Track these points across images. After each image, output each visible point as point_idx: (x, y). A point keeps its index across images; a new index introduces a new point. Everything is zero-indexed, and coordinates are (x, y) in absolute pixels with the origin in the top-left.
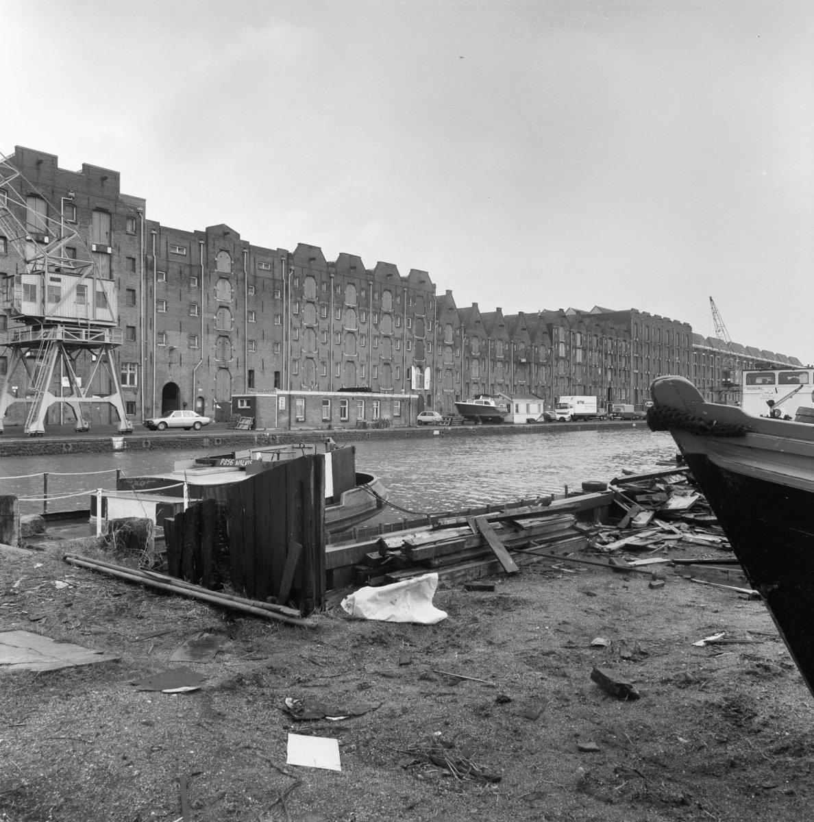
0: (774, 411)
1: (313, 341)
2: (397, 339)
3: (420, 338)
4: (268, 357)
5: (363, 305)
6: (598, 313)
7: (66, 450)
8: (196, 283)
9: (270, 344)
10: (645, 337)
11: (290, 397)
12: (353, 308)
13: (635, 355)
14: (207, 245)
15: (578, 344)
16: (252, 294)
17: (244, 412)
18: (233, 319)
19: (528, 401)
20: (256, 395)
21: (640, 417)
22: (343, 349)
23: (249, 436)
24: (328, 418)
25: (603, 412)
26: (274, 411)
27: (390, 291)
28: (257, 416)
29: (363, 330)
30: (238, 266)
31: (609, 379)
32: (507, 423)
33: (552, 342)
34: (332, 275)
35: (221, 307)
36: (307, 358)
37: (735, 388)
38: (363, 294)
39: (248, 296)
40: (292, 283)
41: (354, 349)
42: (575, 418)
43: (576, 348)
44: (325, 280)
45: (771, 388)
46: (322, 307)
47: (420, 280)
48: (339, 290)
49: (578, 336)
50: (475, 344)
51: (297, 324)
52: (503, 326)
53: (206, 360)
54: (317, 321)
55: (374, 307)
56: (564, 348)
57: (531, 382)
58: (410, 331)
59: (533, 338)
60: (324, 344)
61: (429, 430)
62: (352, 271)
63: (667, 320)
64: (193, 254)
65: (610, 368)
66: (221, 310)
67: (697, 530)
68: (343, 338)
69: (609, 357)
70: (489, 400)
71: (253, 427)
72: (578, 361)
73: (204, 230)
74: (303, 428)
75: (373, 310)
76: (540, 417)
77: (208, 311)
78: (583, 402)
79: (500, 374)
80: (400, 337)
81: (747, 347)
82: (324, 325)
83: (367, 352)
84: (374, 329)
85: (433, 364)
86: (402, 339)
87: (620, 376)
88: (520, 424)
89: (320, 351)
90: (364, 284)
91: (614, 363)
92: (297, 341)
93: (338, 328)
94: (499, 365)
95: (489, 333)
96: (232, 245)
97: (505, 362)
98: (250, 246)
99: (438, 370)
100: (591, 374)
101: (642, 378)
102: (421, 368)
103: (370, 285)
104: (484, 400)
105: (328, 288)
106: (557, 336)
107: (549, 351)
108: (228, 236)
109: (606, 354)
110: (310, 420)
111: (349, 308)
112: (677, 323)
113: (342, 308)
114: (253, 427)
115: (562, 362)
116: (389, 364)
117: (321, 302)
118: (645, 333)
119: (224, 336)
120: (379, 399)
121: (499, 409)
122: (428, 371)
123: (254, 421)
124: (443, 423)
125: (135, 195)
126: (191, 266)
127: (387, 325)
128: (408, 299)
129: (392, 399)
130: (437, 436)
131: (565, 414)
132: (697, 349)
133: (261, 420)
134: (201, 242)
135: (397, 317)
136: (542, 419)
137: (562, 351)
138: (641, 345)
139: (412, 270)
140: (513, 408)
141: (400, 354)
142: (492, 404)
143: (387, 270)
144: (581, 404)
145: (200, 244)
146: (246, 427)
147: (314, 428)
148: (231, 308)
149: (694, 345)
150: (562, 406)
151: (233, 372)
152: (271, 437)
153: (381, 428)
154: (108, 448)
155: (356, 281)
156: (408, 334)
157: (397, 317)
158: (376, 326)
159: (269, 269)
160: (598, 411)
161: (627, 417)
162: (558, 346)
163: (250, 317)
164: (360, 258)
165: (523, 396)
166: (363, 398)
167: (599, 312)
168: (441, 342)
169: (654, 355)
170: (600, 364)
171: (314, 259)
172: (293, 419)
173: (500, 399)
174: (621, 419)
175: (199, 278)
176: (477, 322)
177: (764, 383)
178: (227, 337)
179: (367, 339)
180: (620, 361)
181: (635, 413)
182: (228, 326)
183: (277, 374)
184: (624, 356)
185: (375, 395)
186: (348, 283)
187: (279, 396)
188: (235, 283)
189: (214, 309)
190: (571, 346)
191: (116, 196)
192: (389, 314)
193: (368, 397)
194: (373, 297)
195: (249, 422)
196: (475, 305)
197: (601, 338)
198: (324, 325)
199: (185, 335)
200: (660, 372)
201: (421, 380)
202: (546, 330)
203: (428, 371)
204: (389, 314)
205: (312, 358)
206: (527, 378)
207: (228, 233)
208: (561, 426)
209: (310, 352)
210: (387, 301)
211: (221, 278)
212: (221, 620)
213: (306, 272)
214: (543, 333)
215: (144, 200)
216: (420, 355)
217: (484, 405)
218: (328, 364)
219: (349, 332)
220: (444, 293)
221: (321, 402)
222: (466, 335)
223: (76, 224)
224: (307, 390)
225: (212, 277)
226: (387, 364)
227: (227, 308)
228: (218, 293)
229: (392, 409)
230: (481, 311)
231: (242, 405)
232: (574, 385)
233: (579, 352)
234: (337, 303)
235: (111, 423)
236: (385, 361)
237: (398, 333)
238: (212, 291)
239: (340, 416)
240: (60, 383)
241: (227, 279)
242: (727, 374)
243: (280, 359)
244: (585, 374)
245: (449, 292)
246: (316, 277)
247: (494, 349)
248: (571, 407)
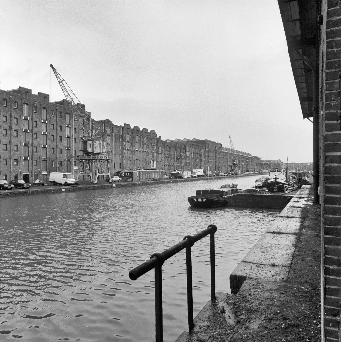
1: (128, 153)
5: (140, 142)
7: (53, 192)
11: (139, 172)
14: (104, 125)
17: (129, 177)
30: (111, 131)
36: (127, 159)
37: (236, 165)
38: (140, 138)
42: (199, 176)
43: (191, 153)
44: (131, 134)
47: (153, 132)
49: (192, 149)
50: (166, 153)
58: (151, 149)
59: (181, 150)
63: (215, 143)
67: (42, 329)
70: (179, 171)
71: (132, 181)
81: (226, 148)
93: (134, 149)
95: (170, 149)
98: (114, 125)
99: (158, 161)
105: (132, 137)
113: (135, 143)
120: (157, 172)
123: (132, 179)
127: (146, 148)
130: (63, 192)
132: (223, 152)
135: (148, 145)
139: (151, 130)
143: (145, 130)
145: (103, 125)
154: (112, 187)
155: (138, 135)
157: (148, 145)
172: (140, 179)
185: (156, 171)
187: (137, 172)
190: (190, 153)
191: (84, 112)
195: (131, 179)
203: (155, 162)
206: (179, 163)
207: (110, 122)
213: (127, 132)
215: (91, 113)
219: (137, 150)
220: (159, 137)
223: (37, 113)
225: (106, 135)
226: (145, 160)
227: (109, 144)
228: (107, 140)
233: (192, 154)
235: (84, 180)
240: (73, 168)
242: (234, 161)
244: (194, 161)
245: (160, 137)
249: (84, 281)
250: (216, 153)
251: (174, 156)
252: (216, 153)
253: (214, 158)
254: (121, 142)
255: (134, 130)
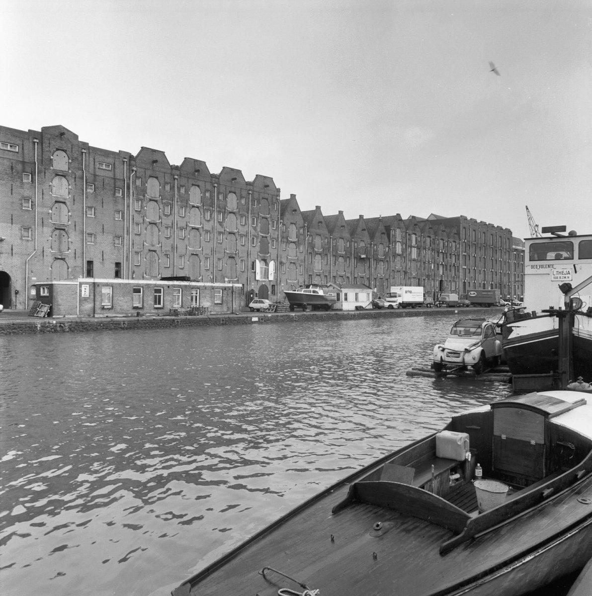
0: (571, 301)
2: (241, 236)
3: (264, 235)
4: (108, 249)
5: (207, 205)
6: (433, 219)
8: (30, 179)
9: (110, 237)
10: (472, 239)
11: (94, 285)
12: (198, 207)
13: (464, 253)
15: (414, 243)
16: (92, 191)
18: (70, 214)
19: (357, 290)
20: (53, 283)
21: (464, 304)
22: (188, 244)
23: (30, 324)
24: (140, 306)
25: (430, 300)
26: (75, 298)
27: (235, 193)
28: (55, 304)
29: (208, 226)
31: (441, 273)
32: (337, 310)
33: (389, 241)
34: (176, 177)
35: (56, 202)
36: (150, 251)
38: (208, 195)
39: (86, 193)
40: (134, 182)
41: (198, 243)
42: (404, 305)
43: (411, 247)
44: (168, 180)
45: (567, 266)
46: (166, 205)
48: (183, 191)
49: (414, 237)
50: (318, 241)
51: (138, 218)
52: (344, 226)
53: (40, 252)
54: (160, 218)
55: (219, 207)
56: (400, 247)
57: (370, 274)
58: (255, 229)
59: (372, 237)
60: (167, 238)
61: (247, 317)
62: (197, 173)
64: (26, 151)
65: (442, 264)
66: (57, 205)
68: (187, 234)
69: (441, 255)
71: (50, 314)
72: (413, 257)
73: (40, 130)
74: (110, 315)
75: (218, 209)
76: (369, 305)
77: (43, 206)
78: (410, 292)
79: (342, 267)
80: (245, 234)
82: (167, 221)
83: (172, 242)
84: (218, 225)
85: (277, 258)
86: (246, 236)
87: (450, 271)
88: (349, 311)
89: (163, 244)
90: (209, 186)
91: (445, 260)
92: (139, 235)
93: (182, 224)
94: (341, 260)
95: (331, 232)
96: (70, 145)
97: (346, 257)
100: (424, 269)
101: (469, 273)
102: (265, 261)
103: (215, 187)
104: (312, 290)
106: (394, 236)
107: (387, 249)
108: (65, 136)
109: (438, 252)
110: (118, 308)
111: (193, 206)
112: (500, 228)
114: (50, 314)
115: (398, 258)
116: (233, 258)
117: (164, 201)
118: (472, 236)
119: (60, 229)
120: (198, 288)
121: (327, 297)
122: (272, 265)
123: (51, 308)
124: (269, 310)
125: (299, 205)
126: (23, 163)
127: (232, 223)
128: (253, 201)
129: (213, 288)
130: (255, 322)
131: (394, 302)
132: (516, 250)
133: (61, 307)
134: (35, 140)
135: (242, 216)
136: (371, 307)
137: (399, 249)
138: (469, 246)
139: (257, 175)
140: (342, 297)
141: (245, 248)
142: (321, 293)
144: (408, 294)
145: (34, 143)
146: (42, 315)
147: (122, 315)
148: (68, 204)
149: (514, 247)
150: (392, 295)
151: (71, 262)
152: (58, 325)
153: (195, 315)
155: (200, 183)
156: (253, 231)
157: (242, 216)
158: (221, 223)
159: (110, 169)
160: (425, 299)
161: (452, 305)
162: (395, 244)
163: (89, 212)
164: (205, 163)
165: (355, 285)
166: (180, 286)
167: (433, 218)
168: (286, 239)
169: (480, 253)
170: (433, 261)
171: (155, 161)
173: (331, 288)
174: (447, 307)
175: (33, 174)
176: (342, 226)
177: (558, 258)
178: (64, 230)
179: (246, 239)
180: (450, 258)
181: (459, 301)
182: (64, 220)
183: (118, 265)
184: (454, 254)
185: (193, 284)
186: (193, 185)
187: (81, 284)
188: (73, 180)
189: (50, 204)
190: (407, 245)
192: (234, 213)
193: (186, 286)
194: (218, 198)
195: (46, 309)
196: (341, 213)
197: (433, 239)
198: (167, 221)
199: (16, 228)
200: (493, 268)
201: (266, 273)
202: (384, 231)
203: (272, 265)
204: (234, 213)
205: (155, 251)
206: (367, 272)
208: (385, 313)
209: (153, 246)
210: (232, 202)
211: (57, 175)
212: (78, 482)
213: (149, 173)
214: (382, 233)
216: (264, 250)
217: (312, 294)
218: (172, 257)
219: (193, 228)
220: (289, 197)
221: (132, 290)
222: (309, 233)
224: (150, 279)
227: (64, 203)
228: (54, 189)
229: (213, 297)
230: (346, 219)
231: (44, 292)
232: (409, 278)
234: (181, 202)
236: (230, 255)
237: (243, 230)
238: (48, 187)
239: (153, 303)
241: (64, 176)
243: (121, 251)
245: (293, 196)
246: (159, 178)
247: (336, 246)
248: (399, 296)
249: (293, 456)
250: (495, 251)
251: (348, 251)
252: (495, 251)
253: (489, 264)
254: (120, 200)
255: (255, 185)
